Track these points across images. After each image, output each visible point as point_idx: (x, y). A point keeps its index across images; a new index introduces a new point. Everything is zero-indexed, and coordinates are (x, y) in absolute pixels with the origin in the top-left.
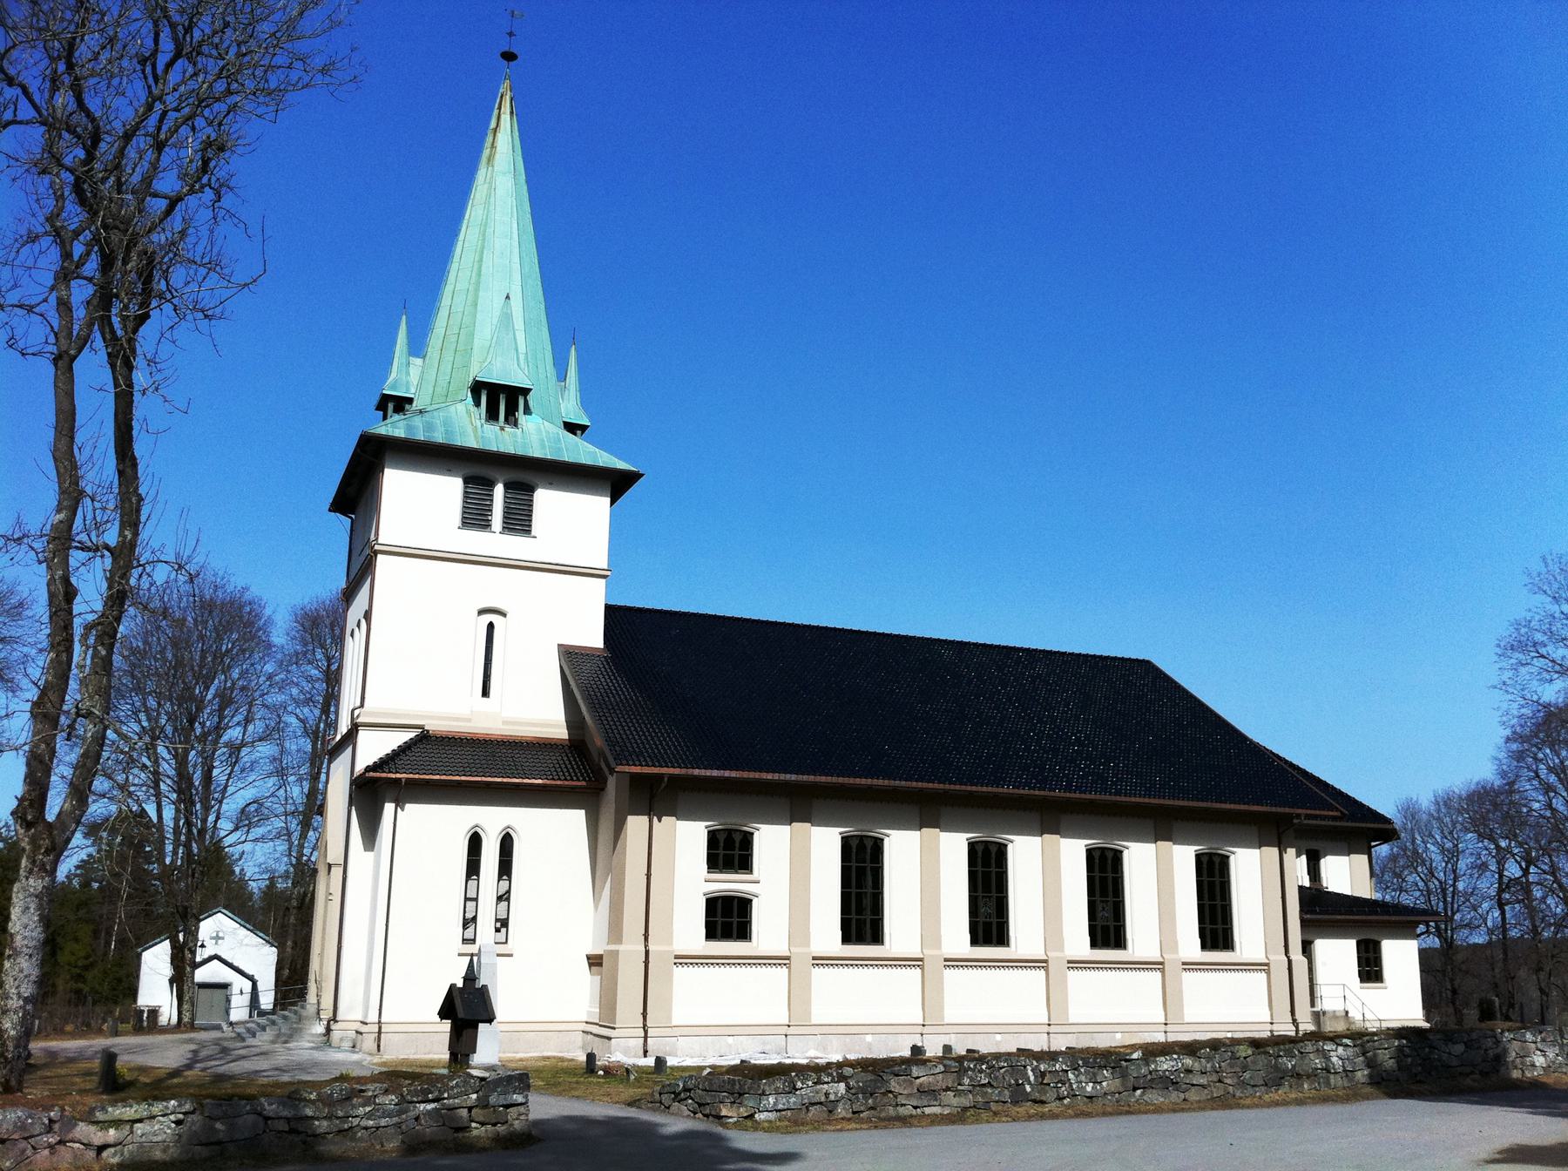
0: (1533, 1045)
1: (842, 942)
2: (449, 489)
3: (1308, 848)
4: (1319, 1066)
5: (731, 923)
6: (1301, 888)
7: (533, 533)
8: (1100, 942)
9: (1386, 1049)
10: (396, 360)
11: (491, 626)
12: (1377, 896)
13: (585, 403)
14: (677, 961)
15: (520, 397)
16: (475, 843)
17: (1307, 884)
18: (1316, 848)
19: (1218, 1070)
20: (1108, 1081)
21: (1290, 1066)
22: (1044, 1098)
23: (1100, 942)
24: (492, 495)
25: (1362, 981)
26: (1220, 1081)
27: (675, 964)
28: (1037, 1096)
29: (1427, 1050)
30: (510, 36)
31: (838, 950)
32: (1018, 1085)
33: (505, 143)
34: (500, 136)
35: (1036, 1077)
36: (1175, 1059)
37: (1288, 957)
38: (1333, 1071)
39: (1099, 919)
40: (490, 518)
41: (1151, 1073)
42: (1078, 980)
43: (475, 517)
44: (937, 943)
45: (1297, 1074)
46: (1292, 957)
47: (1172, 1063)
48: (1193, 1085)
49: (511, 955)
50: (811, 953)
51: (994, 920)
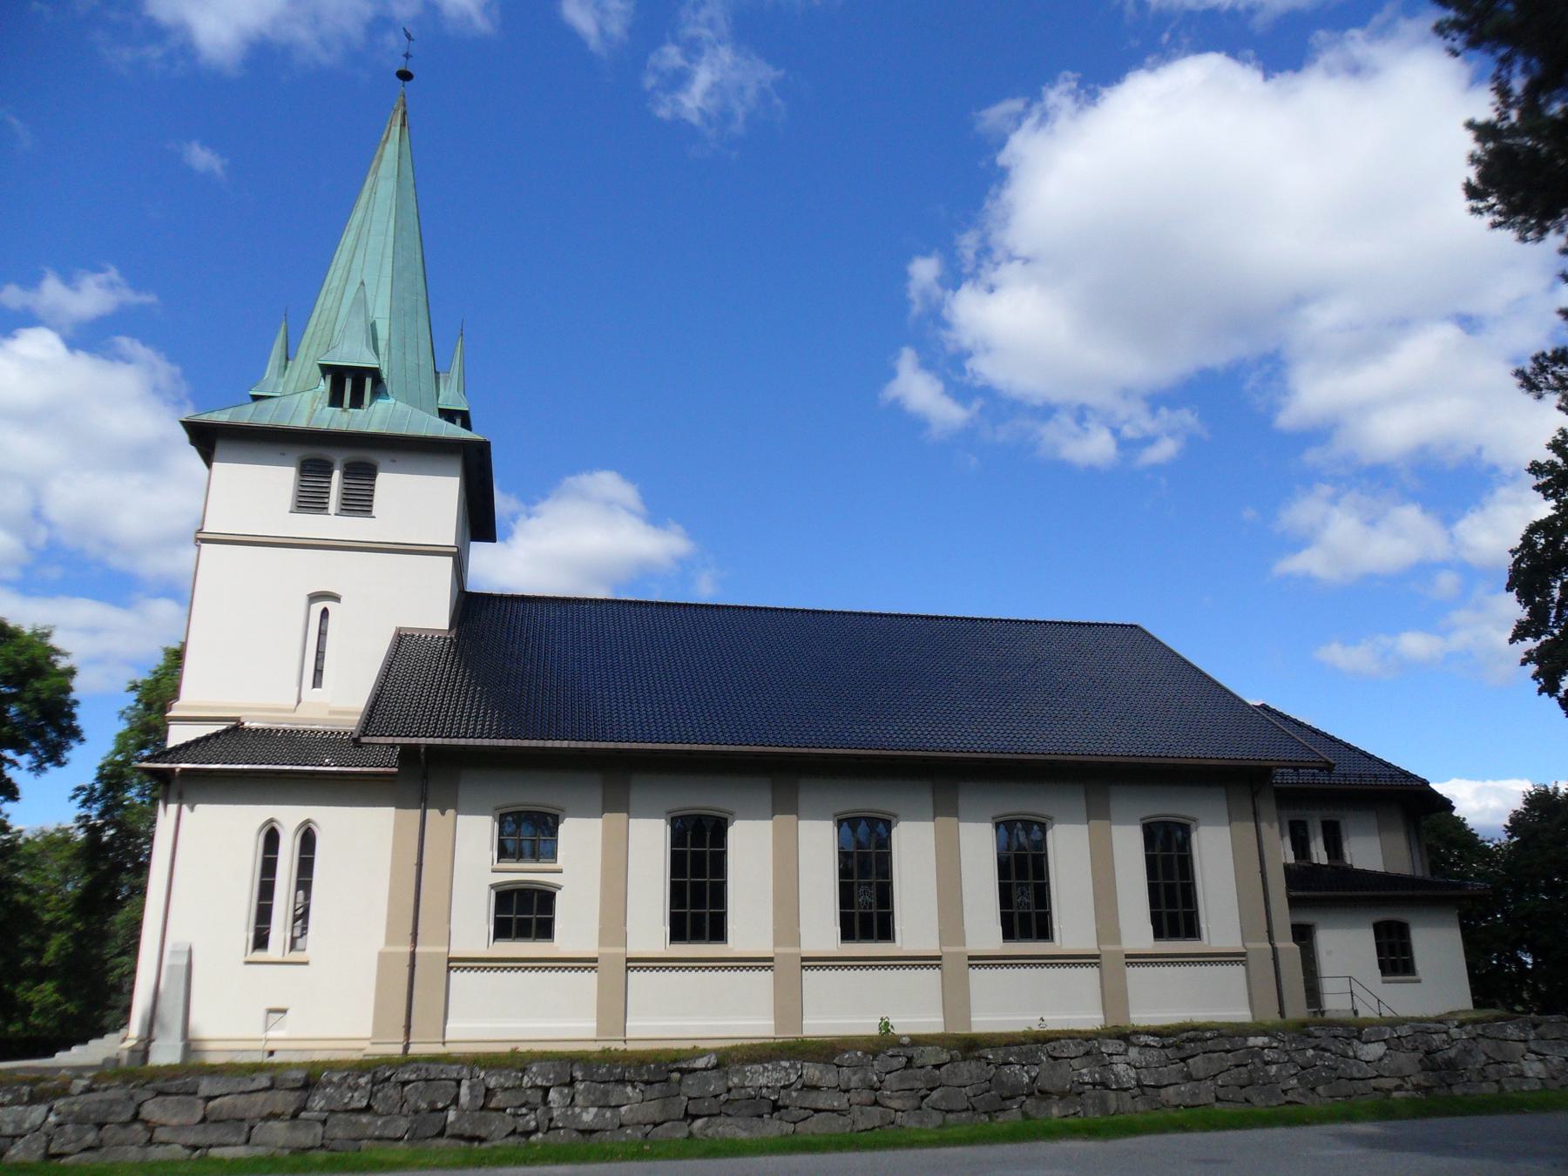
0: (1522, 1046)
1: (1004, 938)
2: (281, 478)
3: (1291, 819)
4: (1087, 1079)
5: (703, 915)
6: (1287, 867)
7: (374, 514)
8: (1017, 930)
9: (1228, 1051)
10: (270, 363)
11: (325, 613)
12: (1428, 875)
13: (464, 388)
14: (971, 962)
15: (347, 380)
16: (271, 839)
17: (1291, 859)
18: (1333, 819)
19: (878, 1085)
20: (633, 1103)
21: (1026, 1079)
22: (482, 1132)
23: (1017, 930)
24: (373, 485)
25: (1384, 972)
26: (876, 1103)
27: (1126, 963)
28: (468, 1129)
29: (1310, 1052)
30: (407, 58)
31: (998, 948)
32: (434, 1110)
33: (390, 150)
34: (388, 146)
35: (473, 1097)
36: (785, 1069)
37: (1272, 945)
38: (1114, 1087)
39: (856, 905)
40: (326, 500)
41: (729, 1090)
42: (1137, 976)
43: (310, 501)
44: (1117, 938)
45: (1039, 1091)
46: (1279, 945)
47: (776, 1075)
48: (817, 1111)
49: (306, 963)
50: (799, 954)
51: (1033, 910)
